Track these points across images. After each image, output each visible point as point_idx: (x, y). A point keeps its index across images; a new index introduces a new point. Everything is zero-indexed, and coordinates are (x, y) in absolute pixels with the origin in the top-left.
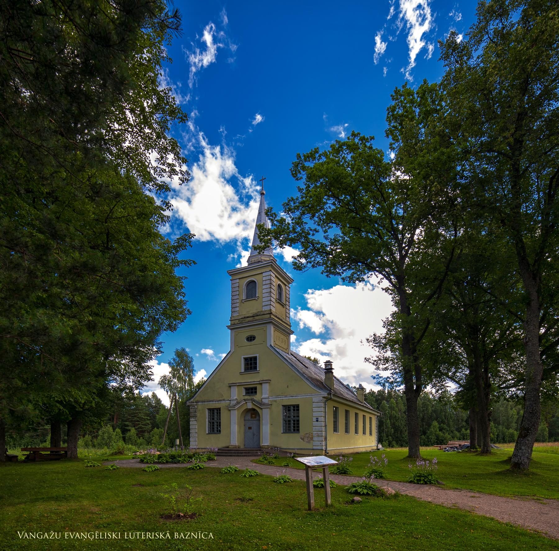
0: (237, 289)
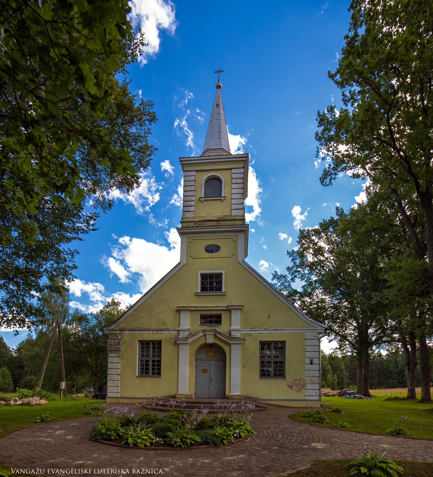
0: (193, 183)
